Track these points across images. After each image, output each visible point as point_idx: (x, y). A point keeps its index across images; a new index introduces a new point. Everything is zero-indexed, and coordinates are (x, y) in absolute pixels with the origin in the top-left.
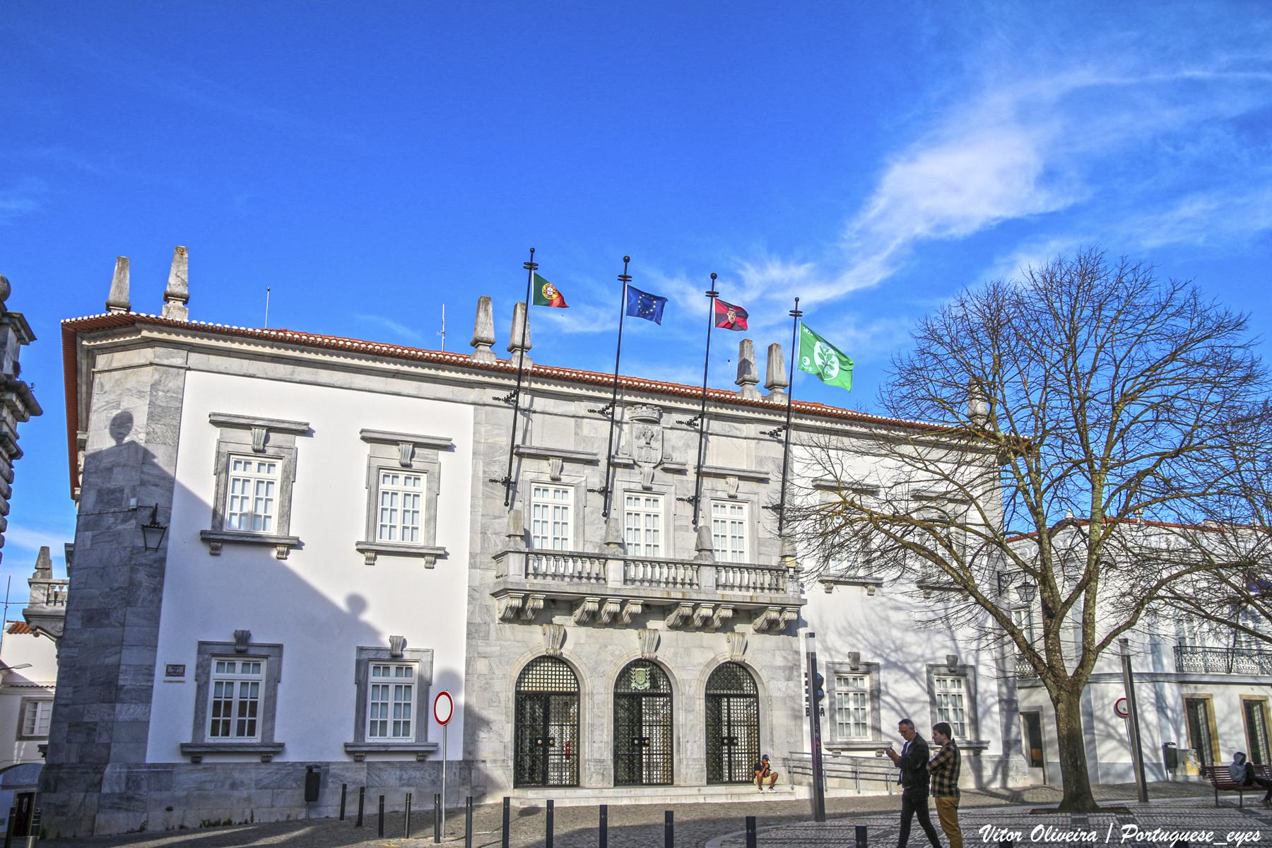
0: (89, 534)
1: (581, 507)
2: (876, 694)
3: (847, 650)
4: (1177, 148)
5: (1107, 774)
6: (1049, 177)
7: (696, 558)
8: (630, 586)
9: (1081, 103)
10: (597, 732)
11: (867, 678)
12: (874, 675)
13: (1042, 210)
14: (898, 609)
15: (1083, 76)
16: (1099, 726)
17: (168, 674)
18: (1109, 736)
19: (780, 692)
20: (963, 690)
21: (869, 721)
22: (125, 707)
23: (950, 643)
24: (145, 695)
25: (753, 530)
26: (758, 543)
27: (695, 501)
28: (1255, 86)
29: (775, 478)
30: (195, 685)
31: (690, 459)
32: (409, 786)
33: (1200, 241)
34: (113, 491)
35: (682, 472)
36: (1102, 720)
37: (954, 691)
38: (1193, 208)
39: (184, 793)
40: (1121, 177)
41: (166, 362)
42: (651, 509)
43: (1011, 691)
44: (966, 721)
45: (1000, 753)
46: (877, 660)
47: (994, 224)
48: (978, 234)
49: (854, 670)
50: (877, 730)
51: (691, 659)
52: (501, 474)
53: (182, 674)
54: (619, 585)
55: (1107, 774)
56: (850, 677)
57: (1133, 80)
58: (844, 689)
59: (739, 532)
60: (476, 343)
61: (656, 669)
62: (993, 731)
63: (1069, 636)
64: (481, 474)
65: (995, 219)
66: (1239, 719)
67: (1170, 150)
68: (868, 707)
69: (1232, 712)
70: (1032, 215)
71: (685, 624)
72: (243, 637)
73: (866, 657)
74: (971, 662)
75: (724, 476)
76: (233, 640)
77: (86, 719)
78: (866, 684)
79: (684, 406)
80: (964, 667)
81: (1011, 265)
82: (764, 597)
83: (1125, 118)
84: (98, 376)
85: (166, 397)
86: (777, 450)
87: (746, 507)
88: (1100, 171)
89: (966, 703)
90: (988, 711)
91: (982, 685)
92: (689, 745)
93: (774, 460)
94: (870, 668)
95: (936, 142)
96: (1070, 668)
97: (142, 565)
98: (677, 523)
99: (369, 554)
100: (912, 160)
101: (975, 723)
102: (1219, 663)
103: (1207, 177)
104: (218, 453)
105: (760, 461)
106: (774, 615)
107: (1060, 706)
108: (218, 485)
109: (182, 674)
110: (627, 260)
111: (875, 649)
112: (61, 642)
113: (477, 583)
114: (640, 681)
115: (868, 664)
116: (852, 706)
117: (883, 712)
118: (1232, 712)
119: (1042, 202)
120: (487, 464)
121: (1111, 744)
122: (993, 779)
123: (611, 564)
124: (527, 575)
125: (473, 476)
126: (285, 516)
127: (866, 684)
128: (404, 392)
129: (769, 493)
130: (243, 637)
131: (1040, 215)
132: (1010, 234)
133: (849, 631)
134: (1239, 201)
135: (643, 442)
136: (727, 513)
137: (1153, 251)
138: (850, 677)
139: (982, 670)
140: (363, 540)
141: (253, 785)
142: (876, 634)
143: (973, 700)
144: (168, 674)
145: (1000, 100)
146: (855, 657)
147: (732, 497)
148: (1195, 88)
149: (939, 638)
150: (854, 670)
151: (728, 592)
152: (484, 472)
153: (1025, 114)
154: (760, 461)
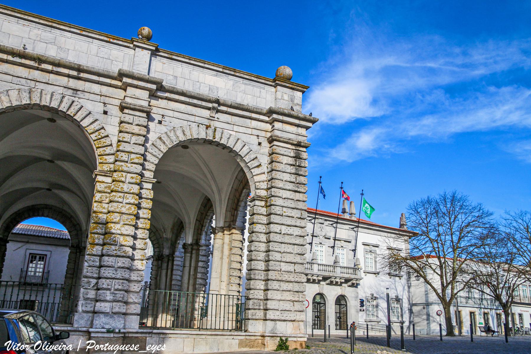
1: (348, 254)
2: (377, 306)
3: (370, 293)
4: (423, 96)
5: (433, 333)
6: (375, 102)
8: (319, 272)
9: (389, 72)
11: (375, 301)
12: (377, 300)
13: (371, 116)
14: (383, 281)
15: (390, 60)
16: (431, 318)
18: (434, 321)
19: (353, 305)
20: (399, 306)
21: (375, 314)
23: (395, 292)
25: (347, 257)
26: (348, 260)
27: (333, 247)
28: (453, 73)
29: (353, 242)
31: (332, 235)
33: (429, 134)
35: (329, 239)
36: (432, 317)
37: (396, 306)
38: (428, 121)
40: (401, 105)
42: (322, 249)
43: (411, 307)
44: (400, 315)
45: (408, 324)
46: (377, 296)
47: (353, 119)
48: (346, 123)
49: (372, 298)
50: (377, 316)
51: (332, 293)
54: (317, 271)
55: (433, 333)
56: (371, 300)
57: (408, 65)
58: (368, 304)
59: (344, 257)
61: (321, 295)
62: (406, 318)
63: (449, 291)
65: (353, 118)
66: (468, 318)
67: (421, 98)
68: (375, 310)
69: (466, 315)
70: (367, 117)
71: (331, 283)
73: (375, 295)
74: (401, 298)
75: (369, 245)
78: (375, 303)
79: (331, 219)
80: (400, 299)
81: (358, 138)
82: (353, 276)
83: (404, 81)
84: (98, 184)
86: (353, 233)
87: (345, 249)
88: (395, 102)
89: (399, 310)
90: (405, 312)
91: (404, 305)
93: (353, 236)
94: (376, 298)
95: (331, 83)
96: (448, 300)
100: (322, 89)
101: (402, 315)
102: (464, 300)
103: (433, 110)
105: (349, 236)
106: (354, 282)
111: (377, 293)
114: (318, 299)
115: (375, 297)
116: (371, 309)
117: (379, 311)
118: (466, 315)
119: (371, 112)
121: (435, 324)
122: (406, 332)
127: (375, 303)
129: (351, 246)
131: (371, 118)
132: (358, 125)
133: (370, 287)
134: (445, 120)
135: (320, 229)
136: (319, 248)
137: (412, 137)
138: (371, 300)
139: (404, 300)
142: (377, 289)
143: (401, 309)
145: (358, 66)
146: (373, 295)
147: (321, 243)
148: (432, 71)
149: (393, 290)
150: (372, 298)
151: (344, 274)
153: (367, 74)
154: (349, 236)
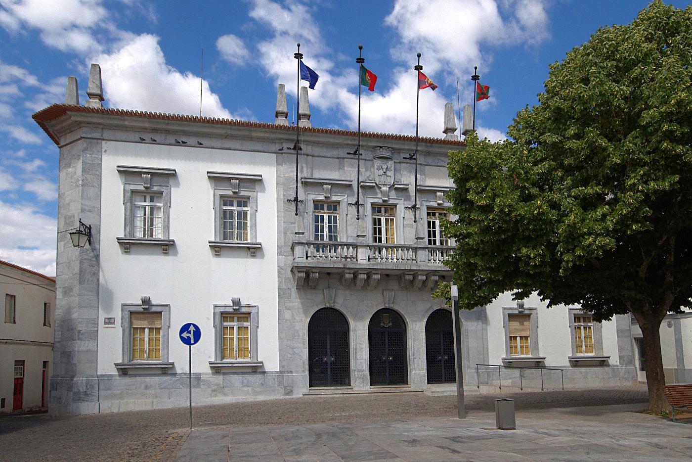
0: (62, 243)
7: (415, 244)
10: (359, 354)
17: (106, 323)
22: (83, 342)
24: (94, 335)
30: (121, 329)
32: (248, 386)
34: (70, 217)
39: (119, 392)
41: (89, 136)
52: (292, 197)
53: (114, 323)
60: (278, 114)
64: (282, 197)
72: (146, 301)
76: (141, 303)
77: (67, 350)
85: (91, 157)
92: (416, 361)
97: (85, 259)
98: (406, 223)
99: (217, 249)
104: (124, 190)
107: (158, 141)
108: (125, 210)
109: (114, 323)
110: (361, 48)
112: (486, 304)
113: (282, 264)
114: (386, 323)
120: (285, 190)
123: (360, 250)
124: (307, 257)
125: (277, 198)
126: (167, 228)
128: (233, 148)
130: (146, 301)
135: (381, 172)
140: (213, 240)
141: (157, 386)
144: (106, 323)
152: (284, 195)
